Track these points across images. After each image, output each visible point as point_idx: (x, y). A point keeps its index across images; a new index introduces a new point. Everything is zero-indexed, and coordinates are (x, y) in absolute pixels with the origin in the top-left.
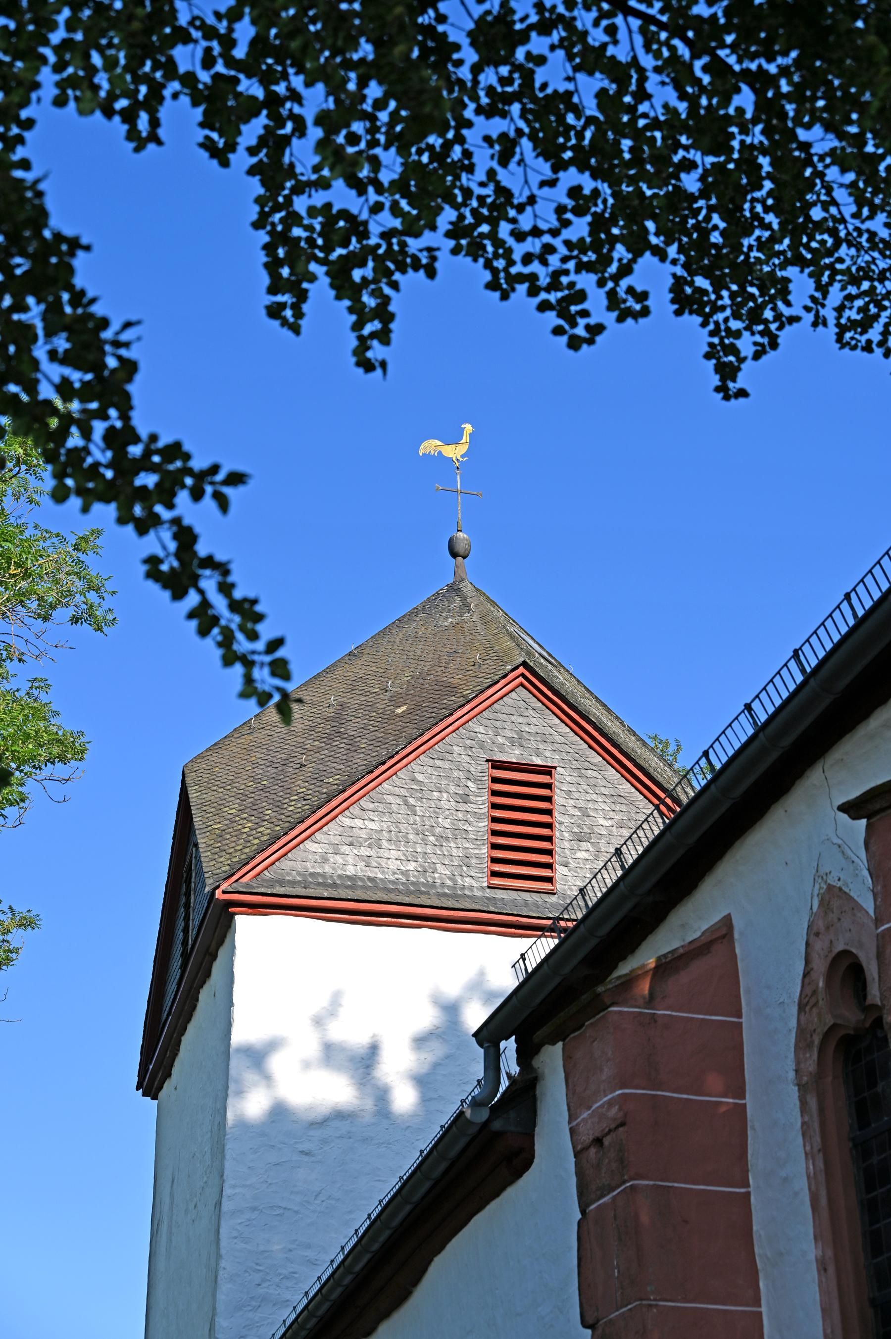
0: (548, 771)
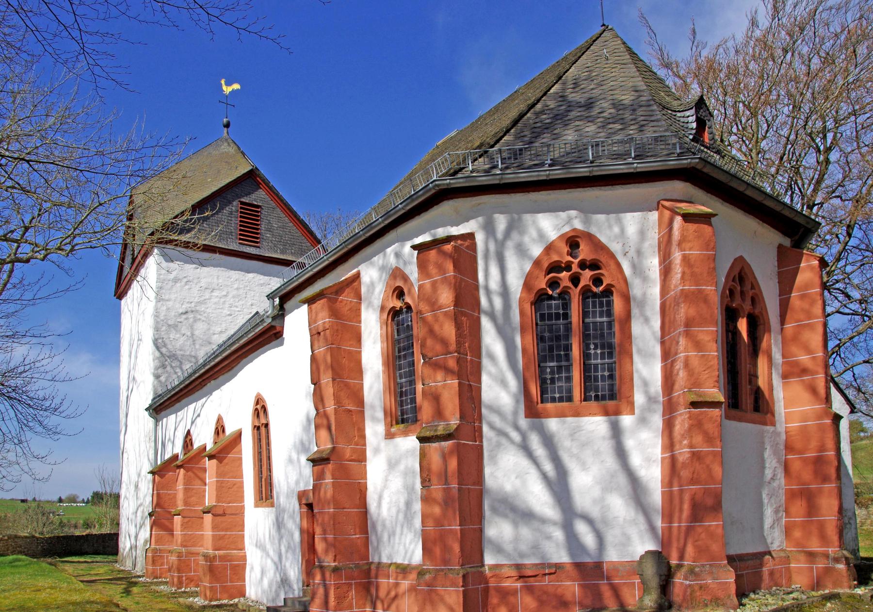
0: (258, 207)
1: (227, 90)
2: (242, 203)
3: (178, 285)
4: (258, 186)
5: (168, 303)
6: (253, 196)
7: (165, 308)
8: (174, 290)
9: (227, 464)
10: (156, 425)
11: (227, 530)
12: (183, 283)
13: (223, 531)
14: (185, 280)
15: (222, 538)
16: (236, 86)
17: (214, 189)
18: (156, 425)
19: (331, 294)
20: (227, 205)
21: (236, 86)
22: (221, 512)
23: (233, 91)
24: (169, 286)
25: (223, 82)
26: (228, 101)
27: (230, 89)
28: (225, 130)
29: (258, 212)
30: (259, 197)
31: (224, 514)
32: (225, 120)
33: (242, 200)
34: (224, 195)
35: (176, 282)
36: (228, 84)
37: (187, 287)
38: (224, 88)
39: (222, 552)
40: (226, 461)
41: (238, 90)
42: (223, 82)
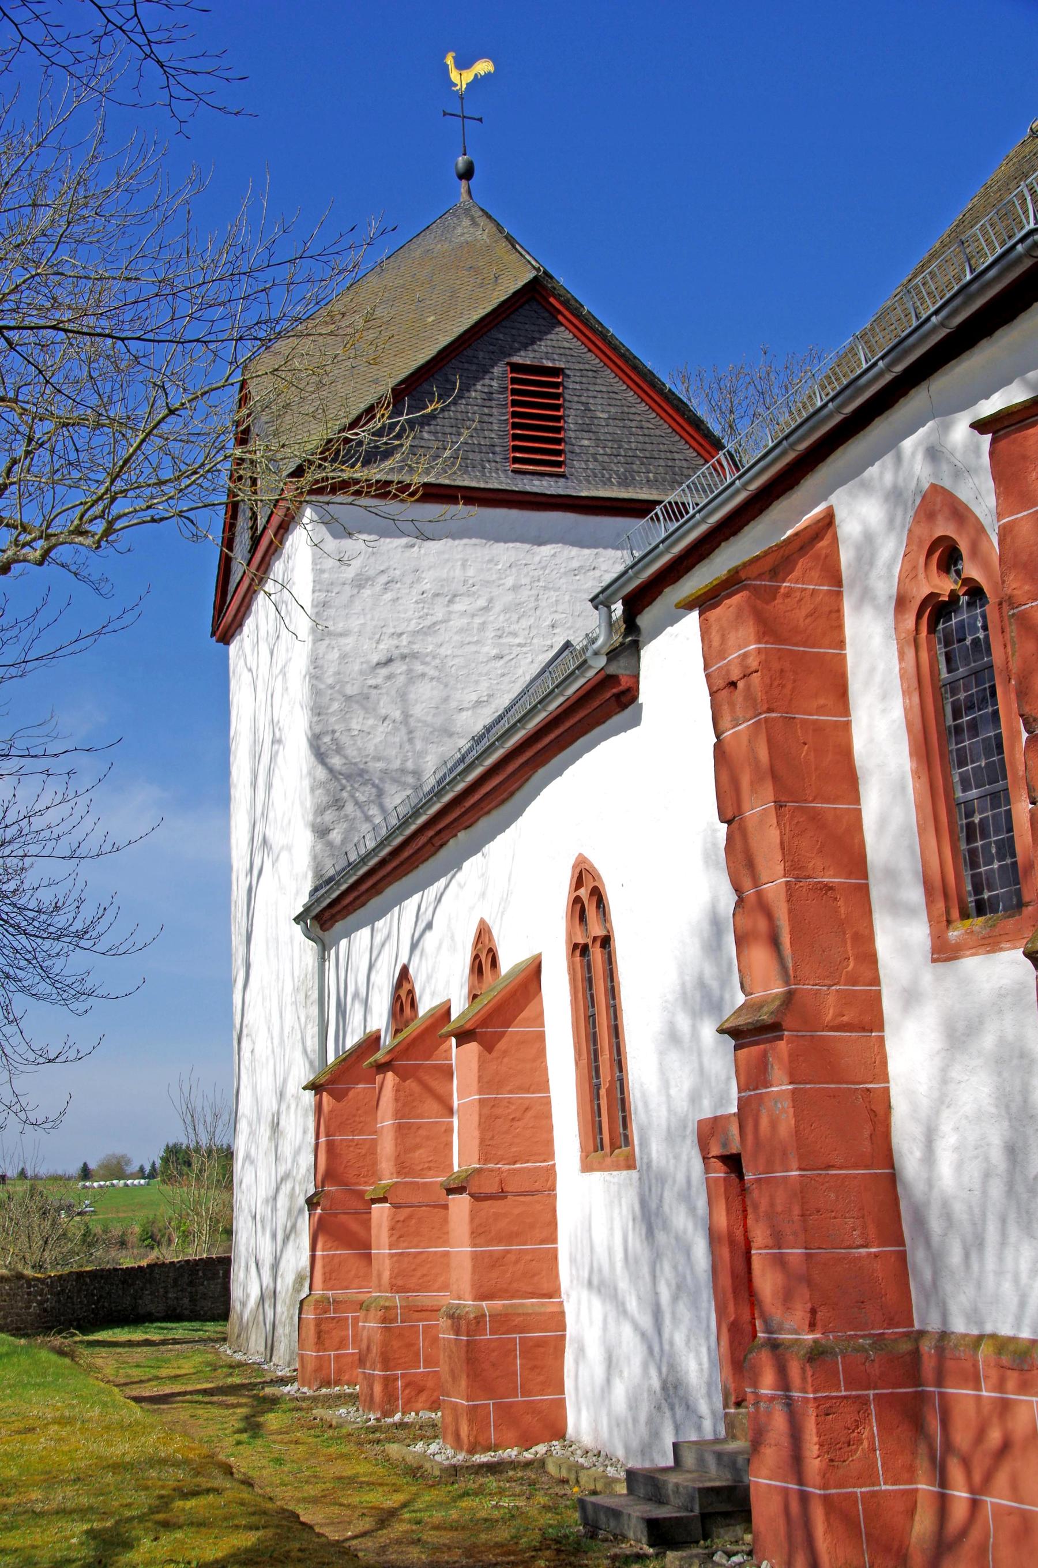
0: (556, 372)
1: (461, 79)
2: (515, 367)
3: (367, 592)
4: (553, 320)
5: (343, 641)
6: (542, 346)
7: (335, 655)
8: (357, 606)
9: (505, 1053)
10: (323, 959)
11: (511, 1238)
12: (378, 588)
13: (499, 1241)
14: (383, 579)
15: (496, 1262)
16: (484, 67)
17: (444, 341)
18: (323, 959)
19: (759, 577)
20: (477, 379)
21: (484, 67)
22: (493, 1188)
23: (478, 81)
24: (344, 598)
25: (450, 61)
26: (462, 109)
27: (468, 76)
28: (464, 183)
29: (556, 385)
30: (556, 347)
31: (501, 1195)
32: (461, 161)
33: (516, 359)
34: (469, 352)
35: (360, 587)
36: (463, 65)
37: (389, 596)
38: (454, 75)
39: (498, 1304)
40: (502, 1045)
41: (488, 75)
42: (450, 61)
